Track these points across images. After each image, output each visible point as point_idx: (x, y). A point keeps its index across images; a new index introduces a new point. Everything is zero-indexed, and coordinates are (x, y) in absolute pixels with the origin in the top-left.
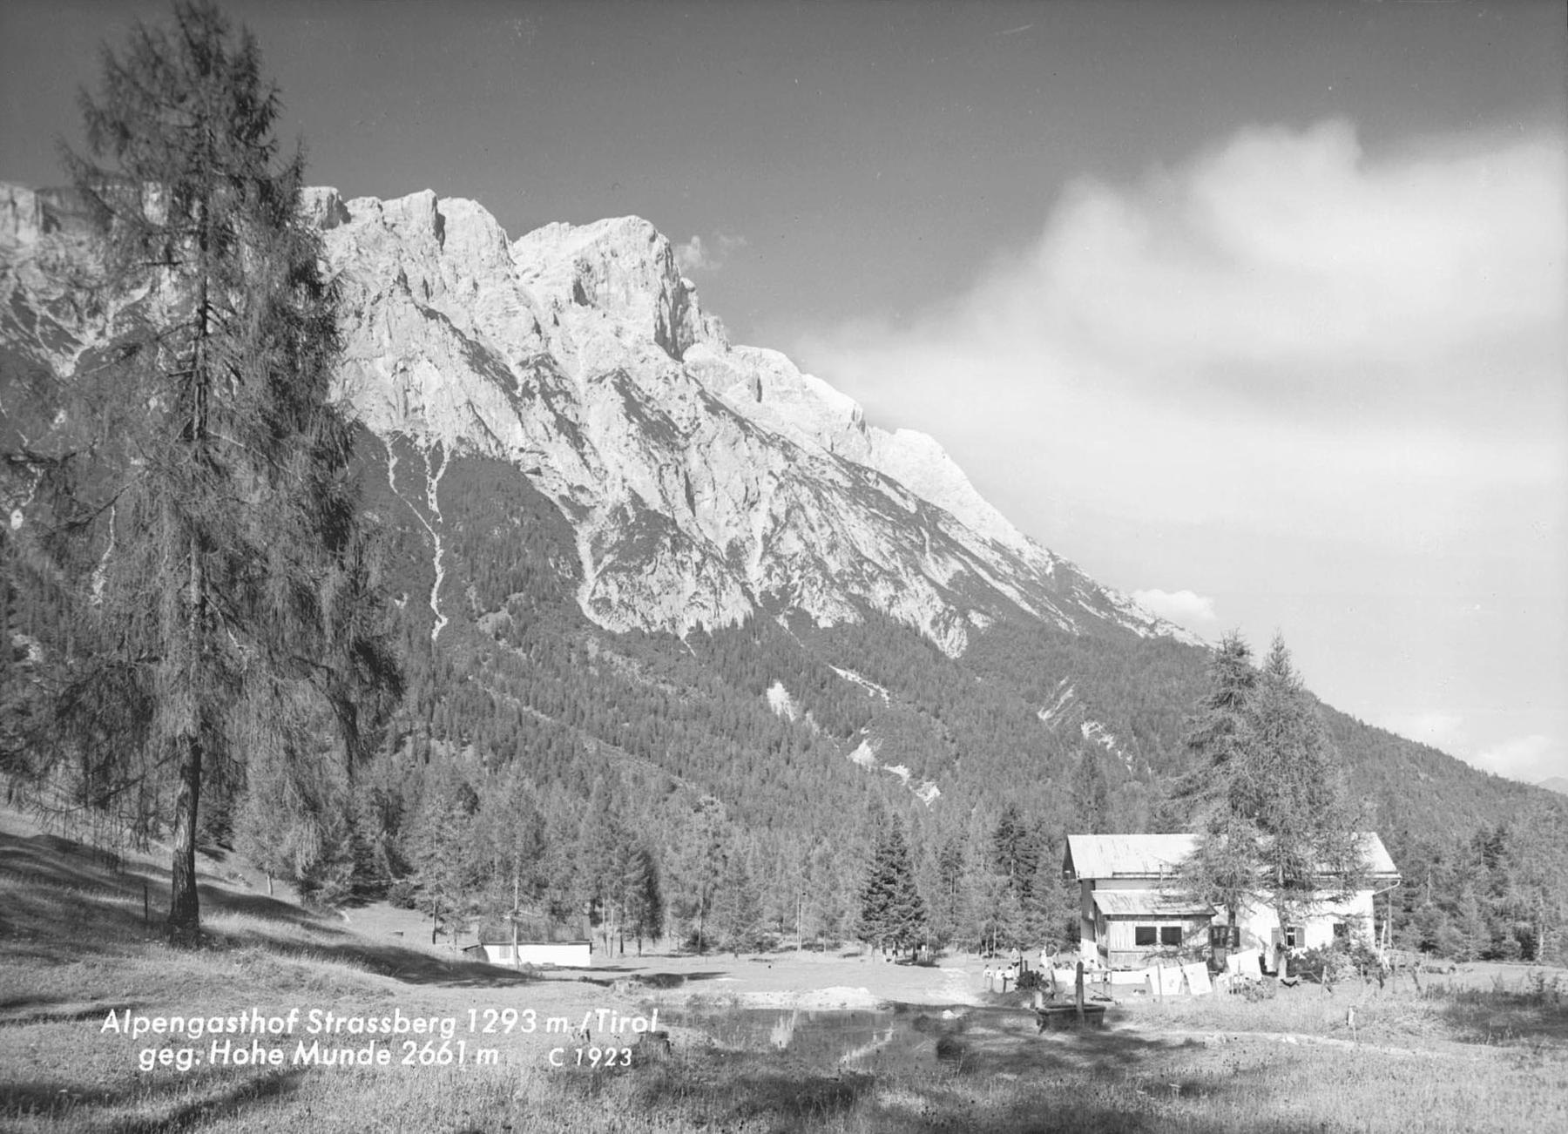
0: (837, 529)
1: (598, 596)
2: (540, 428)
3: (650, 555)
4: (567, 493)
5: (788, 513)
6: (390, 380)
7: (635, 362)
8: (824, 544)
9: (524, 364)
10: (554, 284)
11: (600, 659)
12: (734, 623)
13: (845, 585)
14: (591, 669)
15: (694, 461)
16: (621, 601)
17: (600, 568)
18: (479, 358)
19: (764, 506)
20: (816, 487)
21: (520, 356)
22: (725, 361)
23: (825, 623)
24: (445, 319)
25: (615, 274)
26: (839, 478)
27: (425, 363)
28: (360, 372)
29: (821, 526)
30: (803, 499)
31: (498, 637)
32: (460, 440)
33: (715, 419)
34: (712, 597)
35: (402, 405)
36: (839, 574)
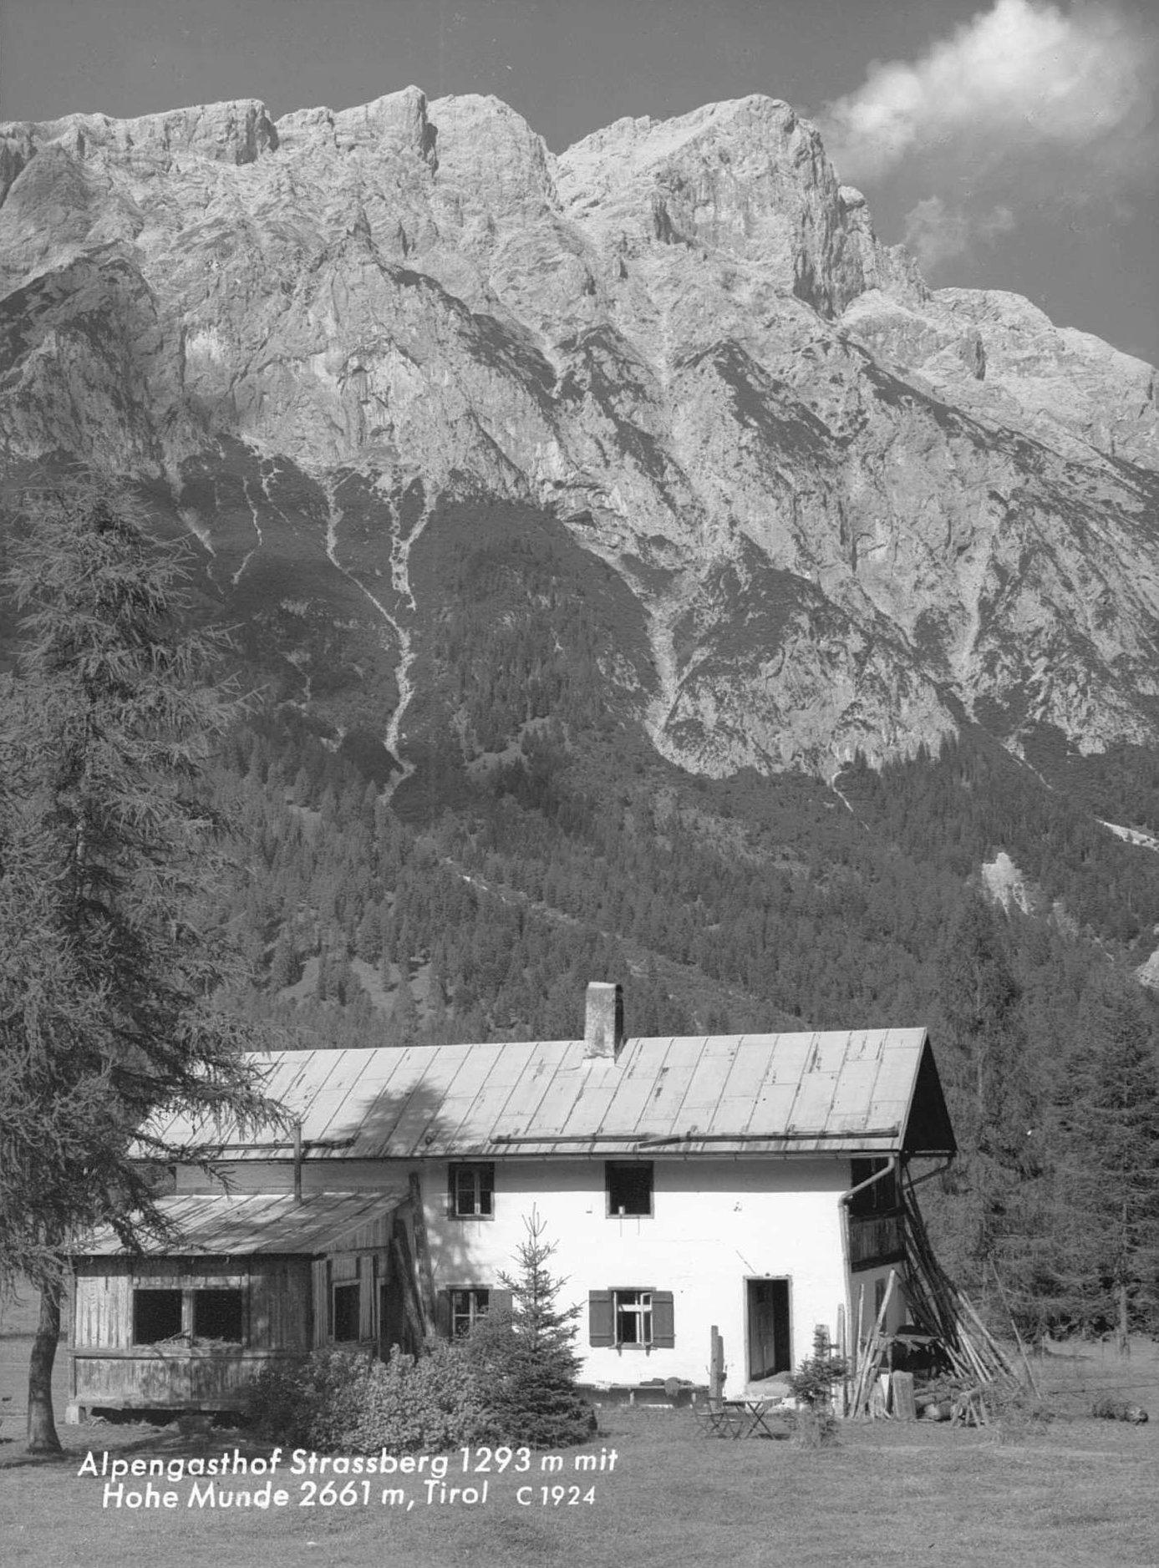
0: (1114, 582)
1: (680, 717)
2: (589, 444)
3: (772, 643)
4: (635, 551)
5: (1025, 561)
6: (336, 390)
7: (757, 326)
8: (1090, 611)
9: (566, 346)
10: (622, 214)
11: (675, 825)
12: (922, 751)
13: (1128, 679)
14: (660, 840)
15: (857, 484)
16: (721, 725)
17: (686, 671)
18: (493, 342)
19: (981, 553)
20: (1076, 515)
21: (560, 331)
22: (920, 316)
23: (1087, 748)
24: (432, 283)
25: (728, 189)
26: (1120, 496)
27: (396, 357)
28: (288, 379)
29: (1085, 581)
30: (1052, 535)
31: (500, 792)
32: (456, 475)
33: (893, 410)
34: (883, 710)
35: (355, 425)
36: (1119, 661)
